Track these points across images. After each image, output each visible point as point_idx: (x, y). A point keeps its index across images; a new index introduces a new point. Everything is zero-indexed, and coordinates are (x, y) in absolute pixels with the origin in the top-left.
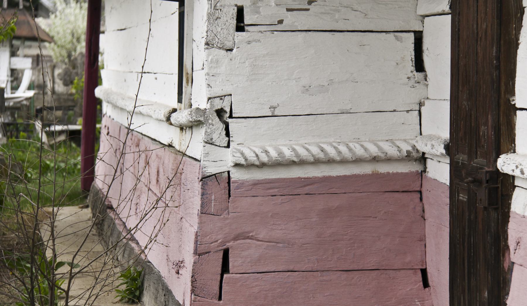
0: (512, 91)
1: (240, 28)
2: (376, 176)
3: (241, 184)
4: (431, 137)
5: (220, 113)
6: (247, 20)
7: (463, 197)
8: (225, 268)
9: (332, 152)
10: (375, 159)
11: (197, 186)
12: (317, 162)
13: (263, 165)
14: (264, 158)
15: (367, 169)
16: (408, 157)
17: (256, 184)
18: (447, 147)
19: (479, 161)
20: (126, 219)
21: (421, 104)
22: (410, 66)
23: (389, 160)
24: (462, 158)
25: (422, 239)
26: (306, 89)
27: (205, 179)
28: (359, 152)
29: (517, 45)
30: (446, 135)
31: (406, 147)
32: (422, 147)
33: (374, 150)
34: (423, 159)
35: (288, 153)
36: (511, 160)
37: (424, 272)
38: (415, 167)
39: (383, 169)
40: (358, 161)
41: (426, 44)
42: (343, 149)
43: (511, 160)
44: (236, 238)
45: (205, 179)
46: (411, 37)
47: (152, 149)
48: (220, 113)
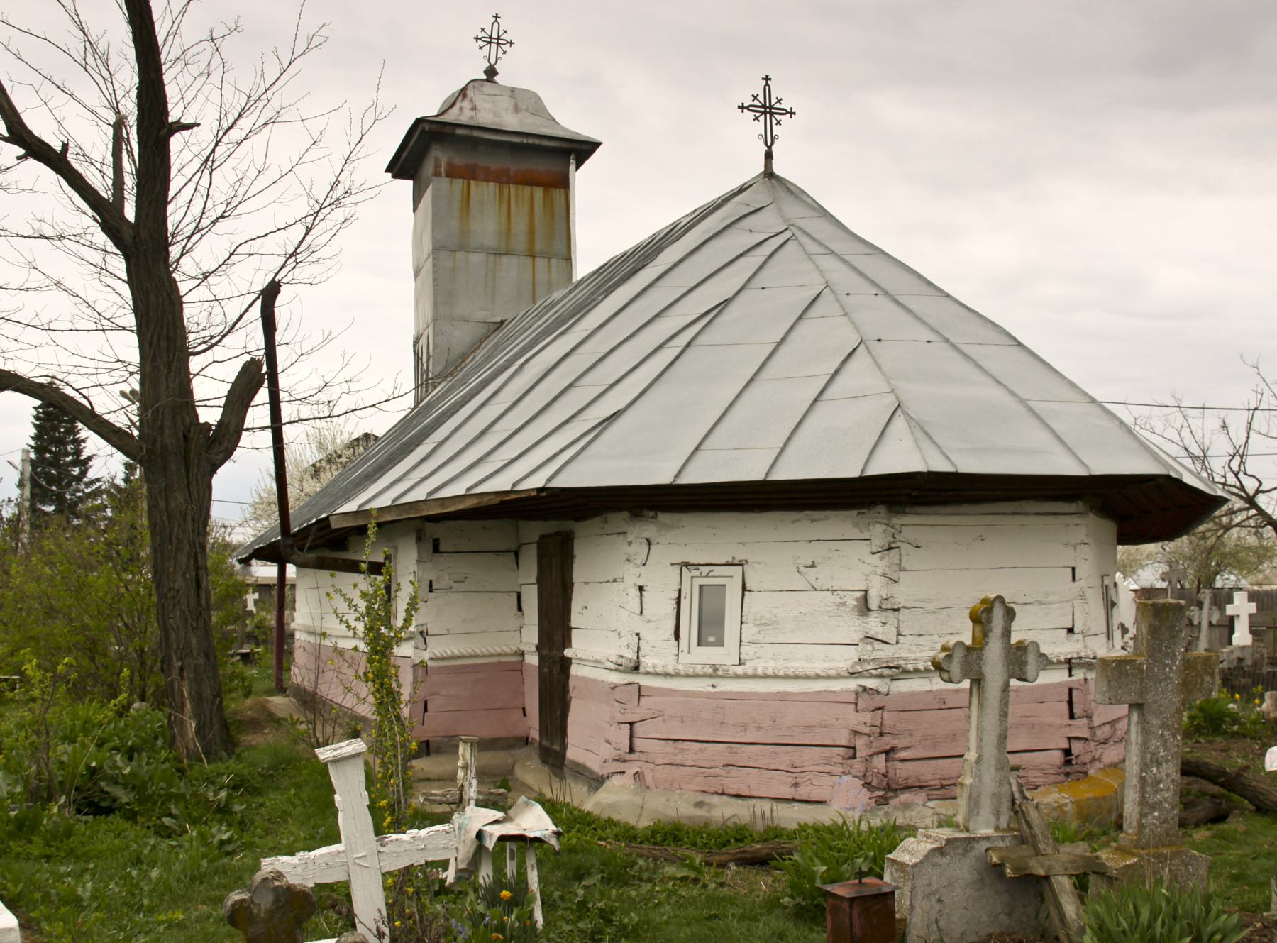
0: (569, 620)
1: (431, 591)
2: (500, 663)
3: (432, 668)
4: (528, 643)
5: (421, 633)
6: (434, 587)
7: (546, 670)
8: (426, 710)
9: (478, 651)
10: (499, 655)
11: (410, 671)
12: (471, 656)
13: (444, 659)
14: (445, 655)
15: (495, 660)
16: (516, 653)
17: (440, 668)
18: (538, 648)
19: (554, 652)
20: (1126, 721)
21: (521, 627)
22: (515, 608)
23: (506, 655)
24: (545, 652)
25: (523, 693)
26: (465, 621)
27: (414, 666)
28: (492, 651)
29: (571, 599)
30: (536, 641)
31: (514, 649)
32: (523, 648)
33: (499, 650)
34: (522, 654)
35: (456, 652)
36: (135, 533)
37: (524, 709)
38: (518, 658)
39: (503, 659)
40: (491, 655)
41: (523, 598)
42: (484, 650)
43: (135, 533)
44: (431, 695)
45: (414, 666)
46: (515, 595)
47: (630, 687)
48: (421, 633)
